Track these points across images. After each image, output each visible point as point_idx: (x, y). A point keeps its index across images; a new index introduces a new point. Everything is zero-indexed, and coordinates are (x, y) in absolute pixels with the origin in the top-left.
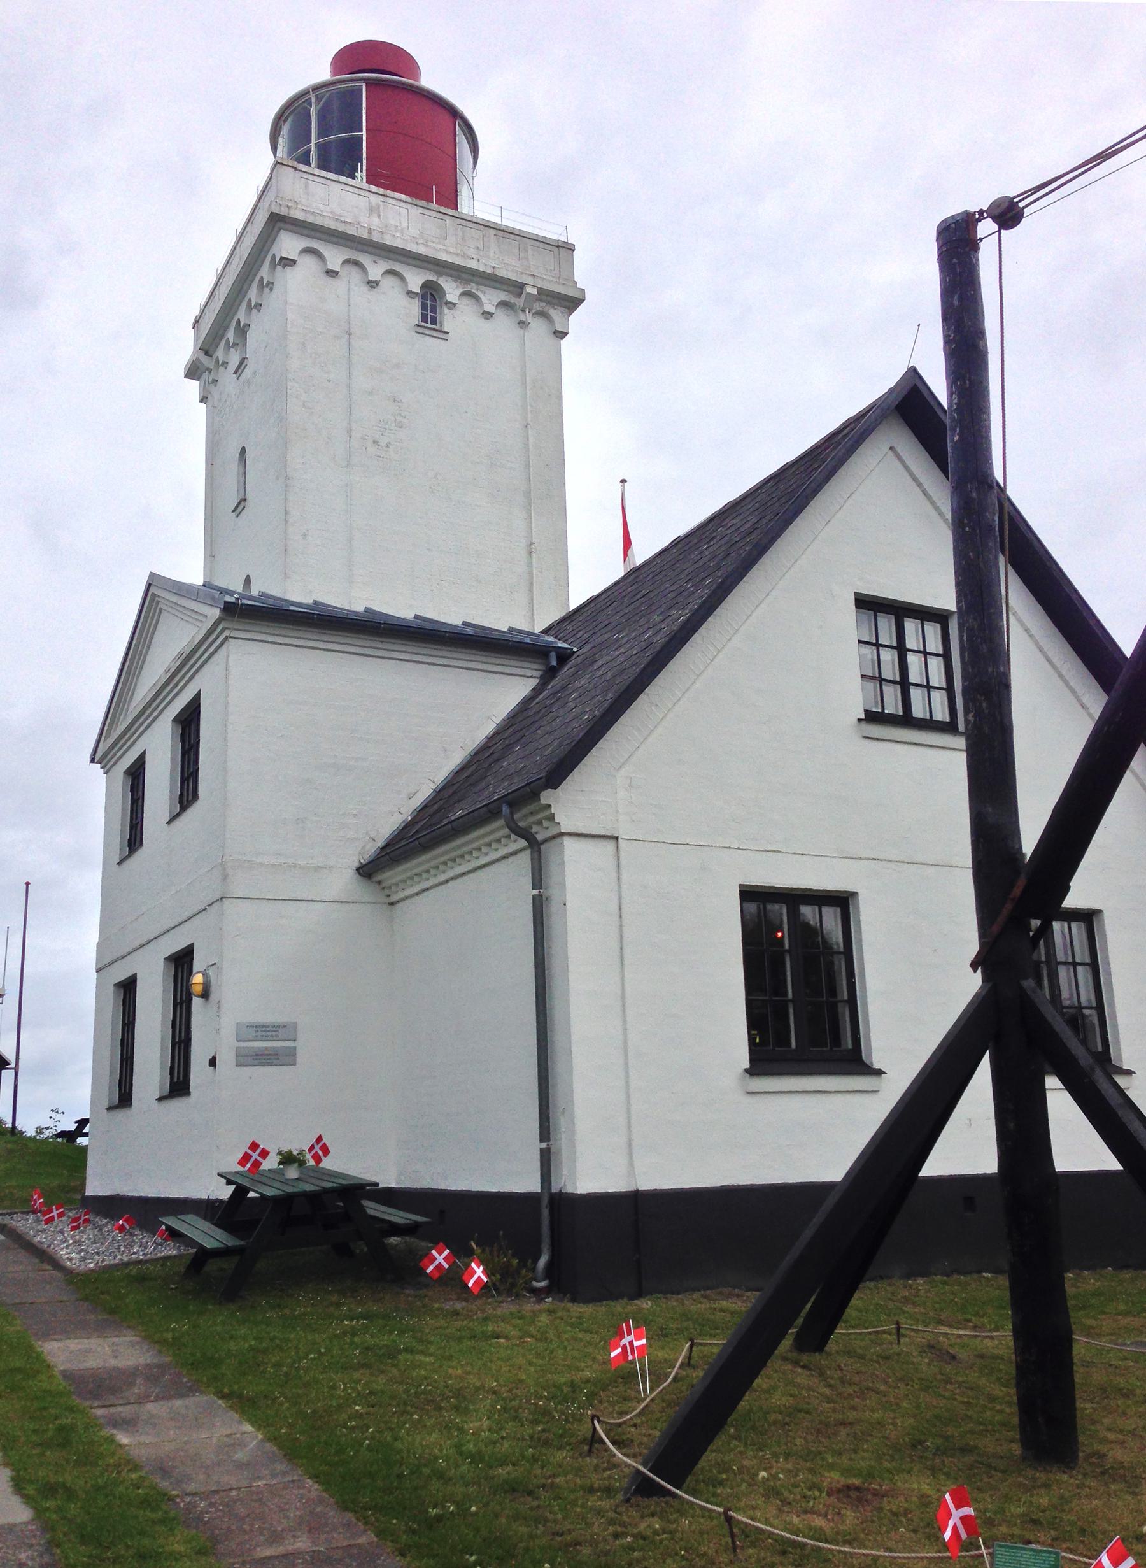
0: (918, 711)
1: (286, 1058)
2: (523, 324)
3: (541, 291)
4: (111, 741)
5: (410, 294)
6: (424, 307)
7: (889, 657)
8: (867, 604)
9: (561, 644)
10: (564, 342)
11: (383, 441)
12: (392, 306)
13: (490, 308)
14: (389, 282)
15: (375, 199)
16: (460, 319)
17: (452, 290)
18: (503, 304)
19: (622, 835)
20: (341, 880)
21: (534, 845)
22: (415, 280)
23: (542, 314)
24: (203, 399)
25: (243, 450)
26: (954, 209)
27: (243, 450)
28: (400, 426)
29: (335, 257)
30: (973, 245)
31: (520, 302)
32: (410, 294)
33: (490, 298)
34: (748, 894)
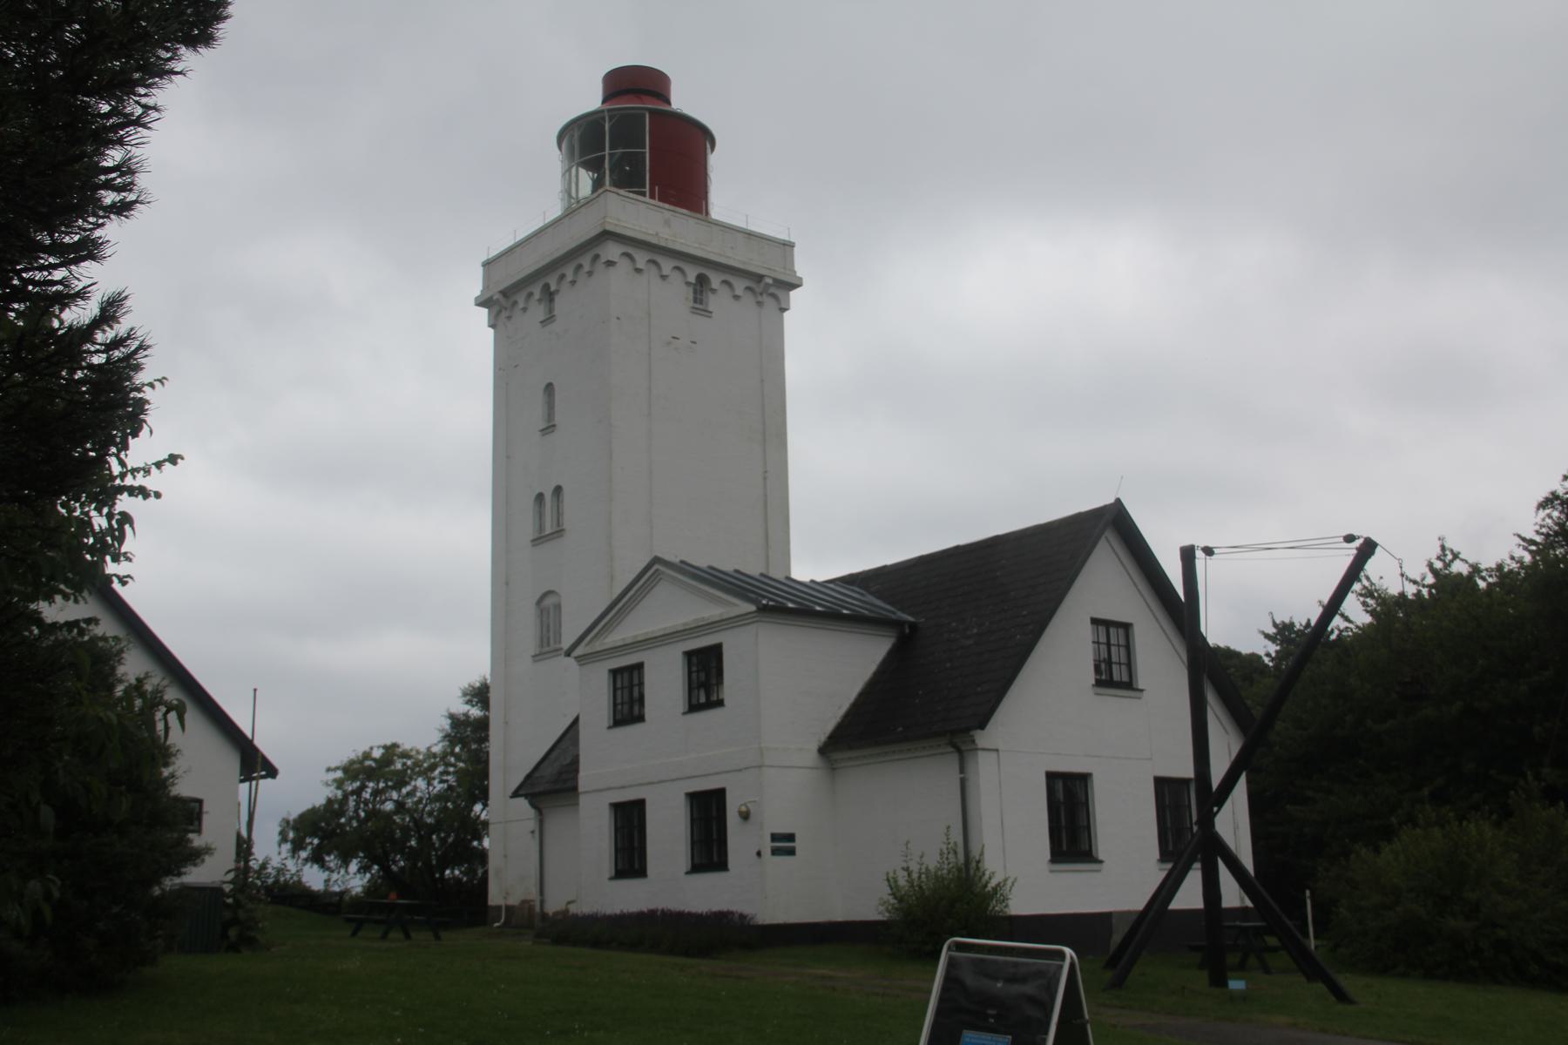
0: (1116, 677)
1: (791, 852)
2: (759, 304)
3: (775, 280)
4: (589, 650)
5: (688, 284)
6: (695, 292)
7: (1103, 648)
8: (1096, 622)
9: (911, 619)
10: (786, 314)
12: (673, 293)
13: (739, 292)
14: (676, 276)
16: (719, 301)
17: (715, 279)
18: (748, 288)
19: (1000, 748)
20: (810, 756)
21: (960, 751)
22: (692, 273)
23: (773, 296)
24: (492, 326)
25: (549, 388)
26: (1187, 543)
27: (549, 388)
29: (641, 258)
30: (1194, 557)
31: (758, 289)
32: (688, 284)
33: (740, 285)
34: (1051, 777)
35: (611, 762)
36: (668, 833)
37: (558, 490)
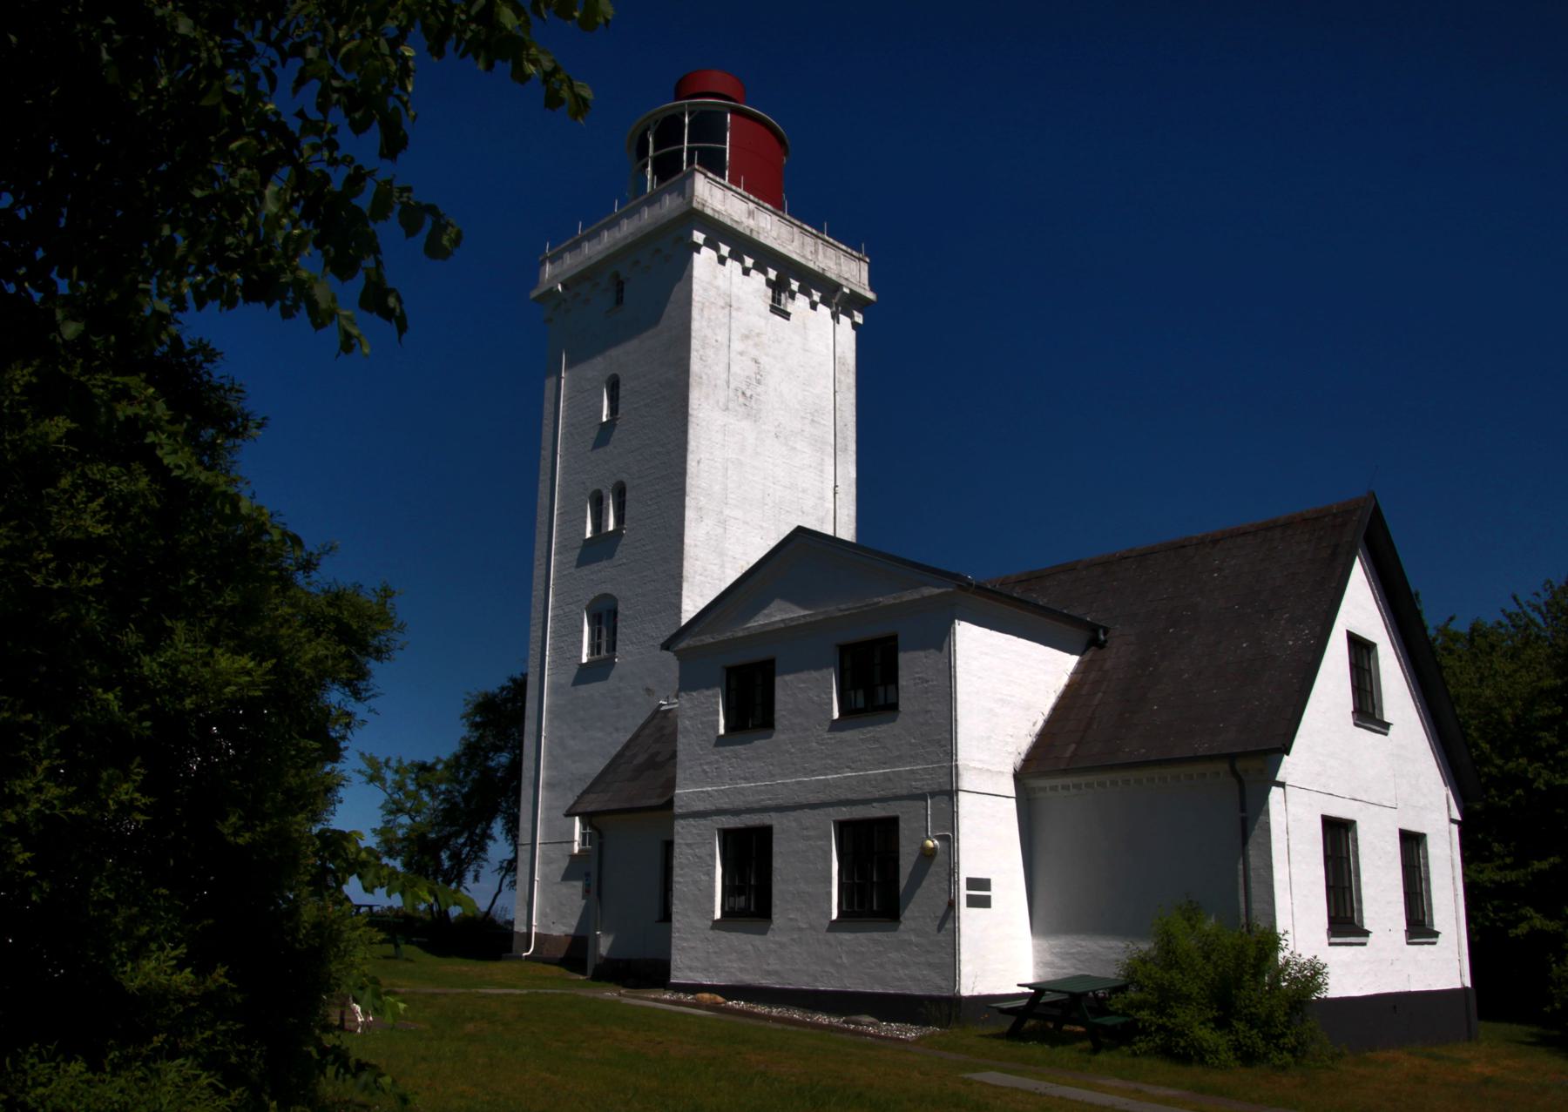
11: (748, 393)
15: (752, 206)
28: (759, 382)
35: (714, 780)
36: (815, 876)
37: (620, 493)
